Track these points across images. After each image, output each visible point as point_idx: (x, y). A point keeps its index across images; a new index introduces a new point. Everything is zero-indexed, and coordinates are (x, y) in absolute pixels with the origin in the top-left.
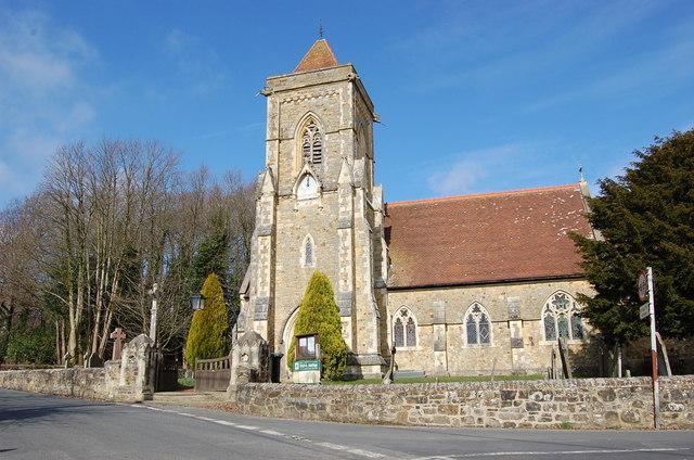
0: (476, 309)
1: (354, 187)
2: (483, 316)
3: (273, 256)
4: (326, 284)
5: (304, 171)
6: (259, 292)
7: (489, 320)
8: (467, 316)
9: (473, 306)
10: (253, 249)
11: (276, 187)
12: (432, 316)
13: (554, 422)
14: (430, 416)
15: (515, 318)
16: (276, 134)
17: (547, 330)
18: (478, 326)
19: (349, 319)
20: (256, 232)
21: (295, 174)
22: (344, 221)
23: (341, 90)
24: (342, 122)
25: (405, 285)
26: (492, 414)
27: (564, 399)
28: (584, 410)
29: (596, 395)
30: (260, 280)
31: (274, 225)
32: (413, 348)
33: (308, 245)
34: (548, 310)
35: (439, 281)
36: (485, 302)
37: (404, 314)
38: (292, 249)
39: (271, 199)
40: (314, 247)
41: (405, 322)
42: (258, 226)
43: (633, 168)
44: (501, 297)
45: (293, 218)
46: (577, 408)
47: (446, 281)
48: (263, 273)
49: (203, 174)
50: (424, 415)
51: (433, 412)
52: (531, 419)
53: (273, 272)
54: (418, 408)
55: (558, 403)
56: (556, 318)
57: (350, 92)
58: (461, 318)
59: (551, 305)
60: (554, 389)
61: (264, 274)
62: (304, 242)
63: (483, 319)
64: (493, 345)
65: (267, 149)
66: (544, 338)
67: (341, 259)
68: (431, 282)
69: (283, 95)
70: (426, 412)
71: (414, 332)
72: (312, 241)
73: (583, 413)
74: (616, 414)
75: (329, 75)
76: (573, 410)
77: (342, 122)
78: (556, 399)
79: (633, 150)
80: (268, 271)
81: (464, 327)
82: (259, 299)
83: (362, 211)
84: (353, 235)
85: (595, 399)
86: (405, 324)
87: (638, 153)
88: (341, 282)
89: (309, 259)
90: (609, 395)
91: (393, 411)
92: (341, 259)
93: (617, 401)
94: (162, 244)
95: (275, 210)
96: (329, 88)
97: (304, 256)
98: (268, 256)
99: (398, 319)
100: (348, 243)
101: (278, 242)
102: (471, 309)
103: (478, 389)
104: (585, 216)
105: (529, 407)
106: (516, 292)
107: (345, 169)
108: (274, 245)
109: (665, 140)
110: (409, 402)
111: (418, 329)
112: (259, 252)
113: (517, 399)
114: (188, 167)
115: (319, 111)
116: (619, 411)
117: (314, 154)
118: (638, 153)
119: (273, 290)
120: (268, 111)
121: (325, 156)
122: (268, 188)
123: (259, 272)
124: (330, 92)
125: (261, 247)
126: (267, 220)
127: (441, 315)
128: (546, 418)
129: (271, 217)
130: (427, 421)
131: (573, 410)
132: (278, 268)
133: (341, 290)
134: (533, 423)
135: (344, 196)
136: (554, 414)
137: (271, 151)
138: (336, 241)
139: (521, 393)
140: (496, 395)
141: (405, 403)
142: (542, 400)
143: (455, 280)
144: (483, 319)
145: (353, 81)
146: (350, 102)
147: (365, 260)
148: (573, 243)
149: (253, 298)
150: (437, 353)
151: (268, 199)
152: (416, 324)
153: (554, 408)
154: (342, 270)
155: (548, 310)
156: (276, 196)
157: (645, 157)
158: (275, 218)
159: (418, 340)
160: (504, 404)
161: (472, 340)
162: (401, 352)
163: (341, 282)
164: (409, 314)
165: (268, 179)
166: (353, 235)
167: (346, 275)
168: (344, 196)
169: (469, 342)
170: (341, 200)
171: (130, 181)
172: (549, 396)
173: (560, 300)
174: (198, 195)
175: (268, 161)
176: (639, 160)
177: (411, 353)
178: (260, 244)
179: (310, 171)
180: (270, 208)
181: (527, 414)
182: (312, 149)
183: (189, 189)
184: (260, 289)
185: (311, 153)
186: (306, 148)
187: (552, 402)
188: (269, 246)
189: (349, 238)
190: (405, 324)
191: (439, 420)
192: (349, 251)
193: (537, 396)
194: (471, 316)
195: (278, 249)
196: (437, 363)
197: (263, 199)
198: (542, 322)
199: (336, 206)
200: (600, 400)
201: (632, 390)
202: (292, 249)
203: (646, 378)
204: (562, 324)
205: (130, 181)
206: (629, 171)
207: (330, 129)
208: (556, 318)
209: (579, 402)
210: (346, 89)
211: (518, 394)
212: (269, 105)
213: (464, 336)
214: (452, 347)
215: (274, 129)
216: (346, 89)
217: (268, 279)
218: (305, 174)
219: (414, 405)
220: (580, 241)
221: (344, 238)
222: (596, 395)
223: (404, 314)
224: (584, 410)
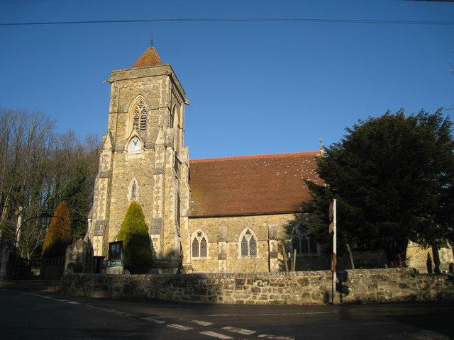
0: (199, 234)
1: (166, 147)
2: (252, 237)
3: (109, 192)
4: (139, 210)
5: (133, 134)
6: (98, 217)
10: (96, 187)
11: (113, 145)
12: (218, 236)
13: (269, 300)
14: (188, 296)
16: (116, 109)
19: (158, 236)
20: (98, 176)
21: (127, 136)
22: (158, 169)
23: (161, 81)
24: (161, 103)
26: (229, 295)
27: (276, 285)
28: (288, 292)
29: (296, 282)
31: (111, 171)
32: (205, 258)
33: (134, 188)
36: (254, 228)
37: (199, 234)
39: (110, 153)
40: (137, 187)
42: (100, 172)
43: (345, 139)
44: (265, 225)
45: (124, 166)
46: (284, 291)
47: (228, 213)
48: (101, 203)
49: (71, 136)
50: (184, 295)
51: (190, 293)
52: (254, 298)
53: (109, 203)
54: (180, 290)
55: (272, 288)
57: (167, 83)
60: (270, 279)
61: (102, 205)
62: (131, 184)
63: (252, 239)
64: (258, 257)
65: (110, 119)
67: (155, 195)
68: (218, 213)
69: (122, 82)
70: (186, 293)
71: (206, 247)
72: (136, 183)
73: (288, 294)
74: (309, 295)
75: (153, 70)
76: (281, 292)
77: (161, 103)
78: (271, 285)
80: (105, 202)
81: (240, 244)
82: (98, 222)
83: (171, 163)
84: (164, 179)
85: (296, 285)
86: (200, 241)
87: (348, 130)
88: (155, 211)
89: (133, 196)
90: (305, 282)
91: (164, 293)
92: (155, 195)
93: (310, 286)
94: (41, 182)
95: (112, 160)
97: (130, 193)
98: (105, 192)
99: (196, 239)
100: (160, 184)
101: (113, 182)
103: (221, 278)
105: (253, 290)
107: (160, 134)
108: (110, 185)
109: (365, 122)
110: (174, 286)
111: (208, 245)
112: (99, 189)
113: (246, 285)
114: (60, 130)
116: (311, 293)
117: (141, 123)
118: (348, 130)
119: (108, 216)
120: (112, 93)
122: (108, 145)
125: (101, 186)
126: (106, 168)
127: (224, 235)
128: (264, 298)
129: (109, 165)
130: (186, 299)
131: (281, 292)
132: (113, 200)
133: (154, 216)
134: (256, 301)
135: (159, 153)
136: (269, 295)
137: (112, 120)
138: (151, 183)
139: (249, 281)
140: (232, 282)
141: (172, 287)
142: (262, 286)
143: (233, 212)
144: (252, 239)
145: (170, 76)
146: (167, 89)
147: (171, 196)
148: (305, 186)
149: (94, 221)
150: (220, 261)
151: (107, 152)
152: (207, 241)
153: (270, 291)
154: (155, 203)
156: (113, 151)
157: (353, 132)
158: (112, 166)
159: (208, 253)
160: (238, 288)
161: (244, 253)
162: (162, 246)
163: (155, 211)
164: (204, 235)
165: (108, 139)
166: (164, 179)
167: (158, 206)
168: (159, 153)
170: (157, 155)
171: (18, 139)
172: (266, 283)
174: (68, 151)
175: (109, 127)
176: (349, 134)
177: (203, 261)
178: (101, 183)
179: (137, 135)
180: (109, 159)
181: (252, 295)
183: (61, 147)
184: (99, 214)
185: (140, 122)
186: (136, 119)
187: (268, 287)
188: (106, 185)
189: (161, 181)
190: (200, 241)
191: (193, 298)
192: (161, 190)
193: (259, 283)
194: (244, 238)
195: (113, 188)
196: (220, 268)
197: (104, 153)
199: (153, 159)
200: (298, 285)
201: (320, 279)
202: (122, 188)
203: (330, 271)
204: (304, 241)
205: (18, 139)
206: (344, 140)
209: (286, 286)
210: (164, 81)
211: (246, 282)
212: (113, 90)
213: (239, 251)
215: (115, 106)
216: (164, 81)
217: (105, 208)
218: (133, 137)
219: (178, 289)
220: (311, 185)
221: (158, 181)
222: (296, 282)
224: (288, 292)
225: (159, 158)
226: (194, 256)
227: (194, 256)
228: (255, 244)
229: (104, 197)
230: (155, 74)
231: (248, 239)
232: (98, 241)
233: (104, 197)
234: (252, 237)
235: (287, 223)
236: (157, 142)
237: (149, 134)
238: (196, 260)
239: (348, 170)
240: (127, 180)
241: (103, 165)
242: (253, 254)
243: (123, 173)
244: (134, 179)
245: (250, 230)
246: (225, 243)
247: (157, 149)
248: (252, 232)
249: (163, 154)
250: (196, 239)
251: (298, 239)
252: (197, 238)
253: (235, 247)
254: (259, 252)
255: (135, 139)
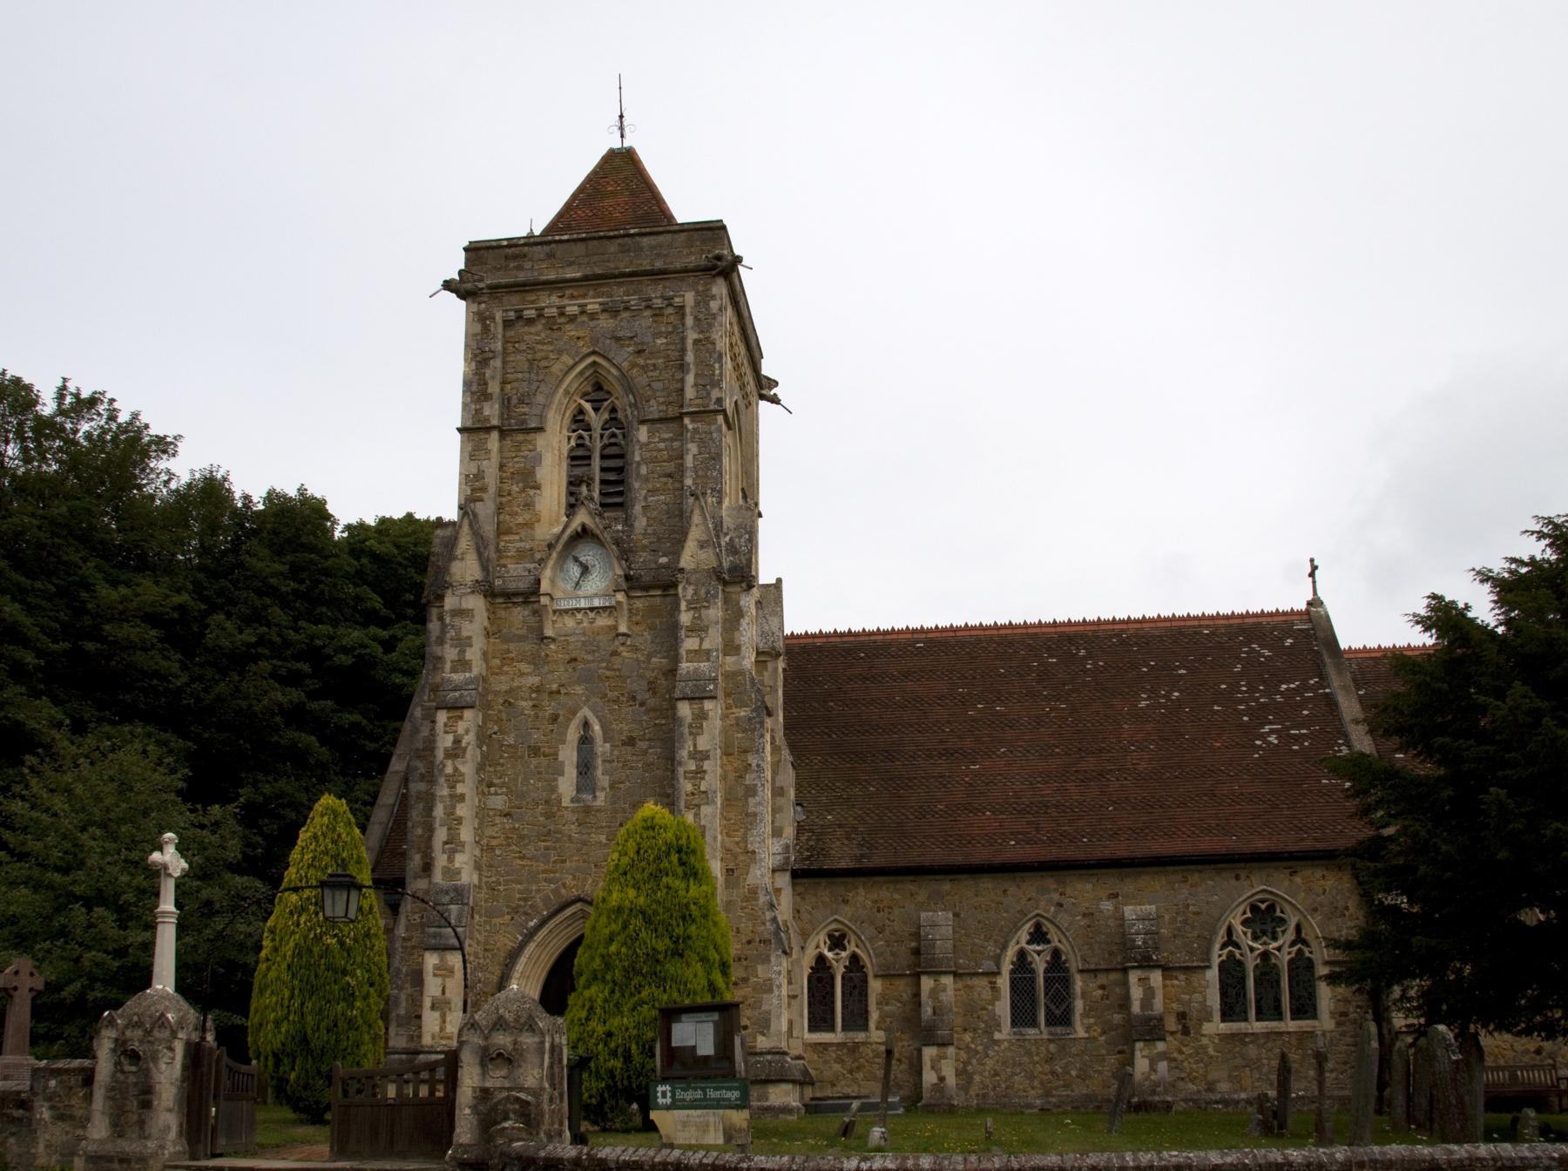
0: (1038, 936)
2: (1056, 953)
5: (576, 524)
7: (1074, 964)
8: (1010, 954)
9: (1028, 927)
15: (1146, 964)
17: (1223, 994)
18: (1041, 981)
24: (690, 393)
25: (843, 865)
30: (441, 835)
32: (860, 1036)
33: (585, 741)
34: (1230, 941)
35: (937, 855)
38: (535, 751)
40: (602, 747)
41: (838, 963)
44: (1107, 906)
45: (538, 661)
48: (450, 812)
56: (1251, 963)
58: (998, 960)
59: (1239, 928)
62: (573, 733)
64: (1081, 1032)
66: (1217, 1016)
79: (182, 447)
81: (1004, 982)
86: (1040, 965)
96: (655, 292)
99: (821, 959)
102: (1023, 935)
104: (1350, 817)
106: (1140, 907)
112: (440, 755)
115: (624, 356)
121: (638, 489)
123: (439, 811)
124: (658, 302)
126: (462, 664)
135: (696, 606)
155: (1230, 941)
159: (874, 1016)
161: (1023, 1015)
168: (696, 606)
169: (1014, 1023)
173: (1264, 919)
177: (853, 1049)
182: (596, 462)
184: (441, 860)
190: (1040, 965)
194: (1022, 954)
198: (1213, 975)
202: (535, 751)
207: (654, 409)
208: (1251, 963)
213: (1003, 1008)
214: (967, 1037)
223: (837, 942)
225: (698, 629)
226: (813, 1028)
227: (813, 1028)
228: (1066, 982)
229: (460, 789)
230: (659, 264)
231: (838, 963)
232: (444, 971)
233: (460, 789)
234: (1056, 953)
235: (1539, 550)
236: (686, 561)
237: (641, 523)
238: (825, 1046)
239: (1014, 1065)
240: (554, 719)
241: (450, 653)
242: (1060, 1017)
243: (538, 690)
244: (586, 712)
245: (1047, 926)
246: (947, 980)
247: (686, 592)
248: (1053, 935)
249: (715, 612)
250: (821, 959)
251: (1240, 963)
252: (830, 955)
253: (987, 994)
254: (1085, 1015)
255: (588, 554)
